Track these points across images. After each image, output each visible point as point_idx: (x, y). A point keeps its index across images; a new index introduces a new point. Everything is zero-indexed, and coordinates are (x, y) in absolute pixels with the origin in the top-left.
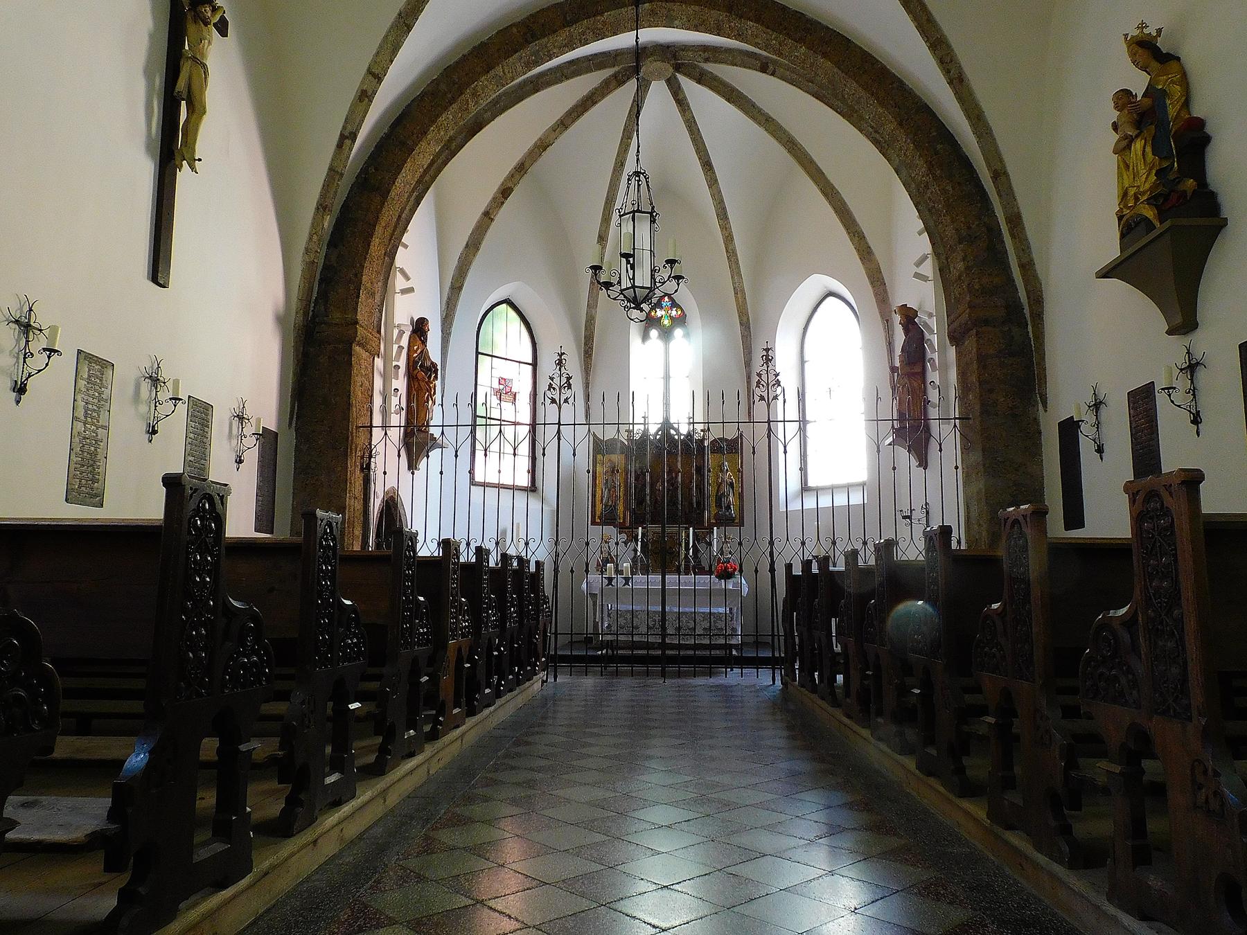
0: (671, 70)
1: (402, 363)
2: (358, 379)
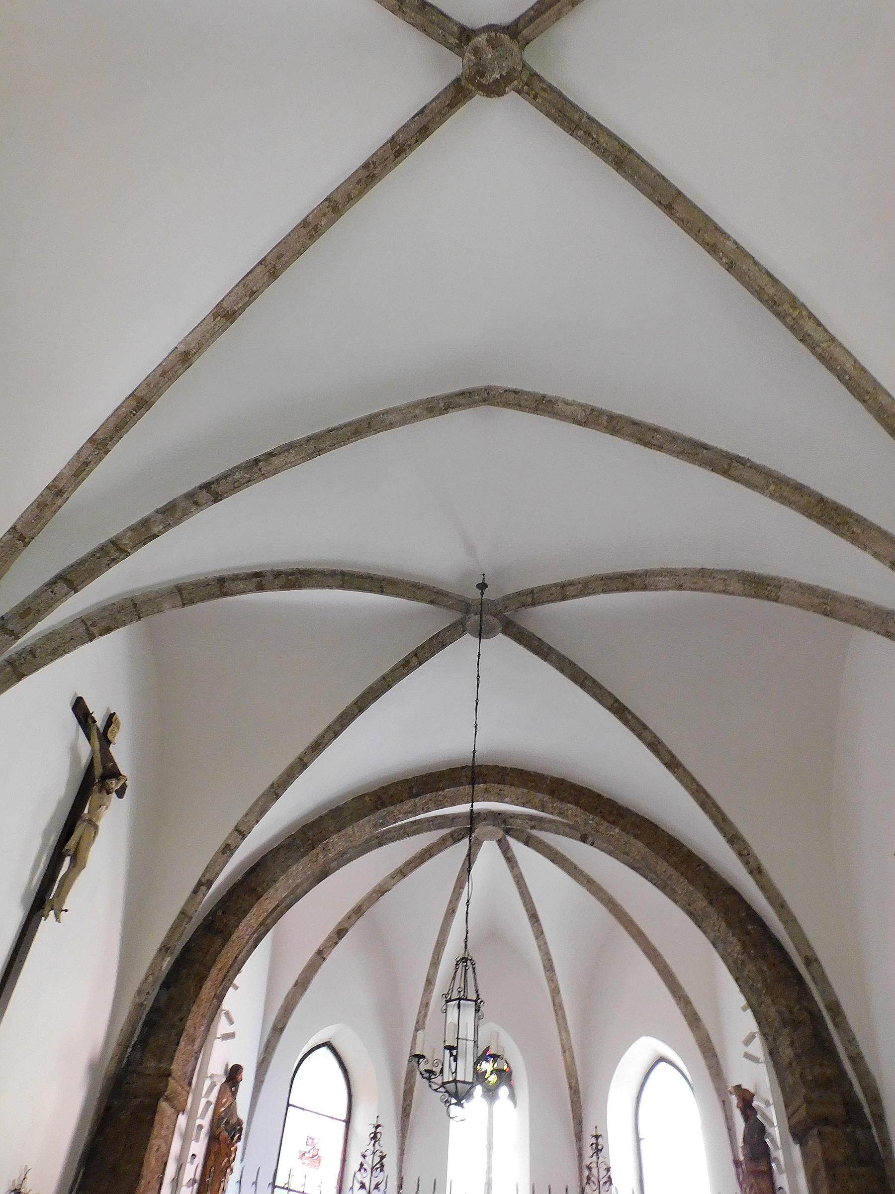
0: (502, 833)
1: (206, 1122)
2: (155, 1142)
